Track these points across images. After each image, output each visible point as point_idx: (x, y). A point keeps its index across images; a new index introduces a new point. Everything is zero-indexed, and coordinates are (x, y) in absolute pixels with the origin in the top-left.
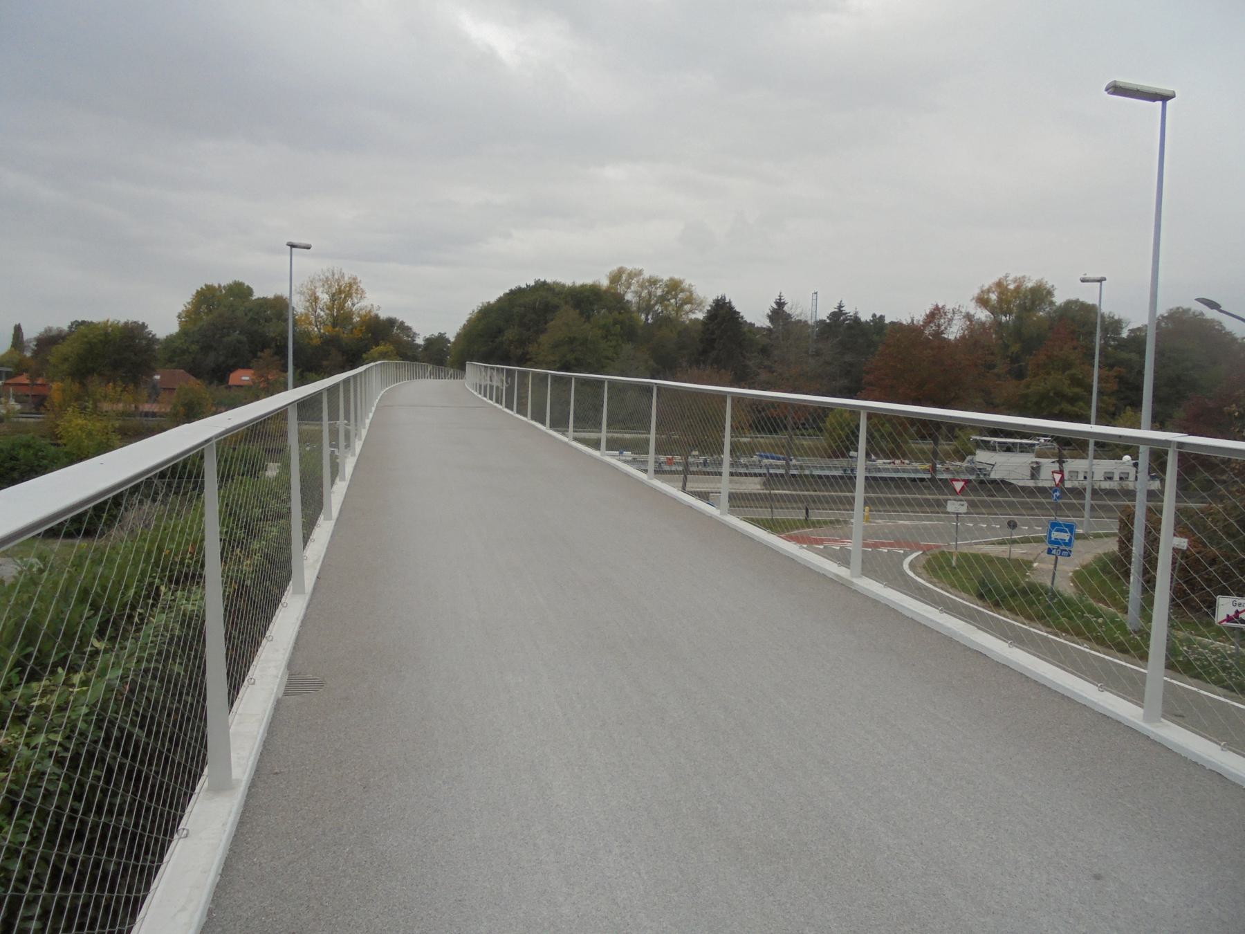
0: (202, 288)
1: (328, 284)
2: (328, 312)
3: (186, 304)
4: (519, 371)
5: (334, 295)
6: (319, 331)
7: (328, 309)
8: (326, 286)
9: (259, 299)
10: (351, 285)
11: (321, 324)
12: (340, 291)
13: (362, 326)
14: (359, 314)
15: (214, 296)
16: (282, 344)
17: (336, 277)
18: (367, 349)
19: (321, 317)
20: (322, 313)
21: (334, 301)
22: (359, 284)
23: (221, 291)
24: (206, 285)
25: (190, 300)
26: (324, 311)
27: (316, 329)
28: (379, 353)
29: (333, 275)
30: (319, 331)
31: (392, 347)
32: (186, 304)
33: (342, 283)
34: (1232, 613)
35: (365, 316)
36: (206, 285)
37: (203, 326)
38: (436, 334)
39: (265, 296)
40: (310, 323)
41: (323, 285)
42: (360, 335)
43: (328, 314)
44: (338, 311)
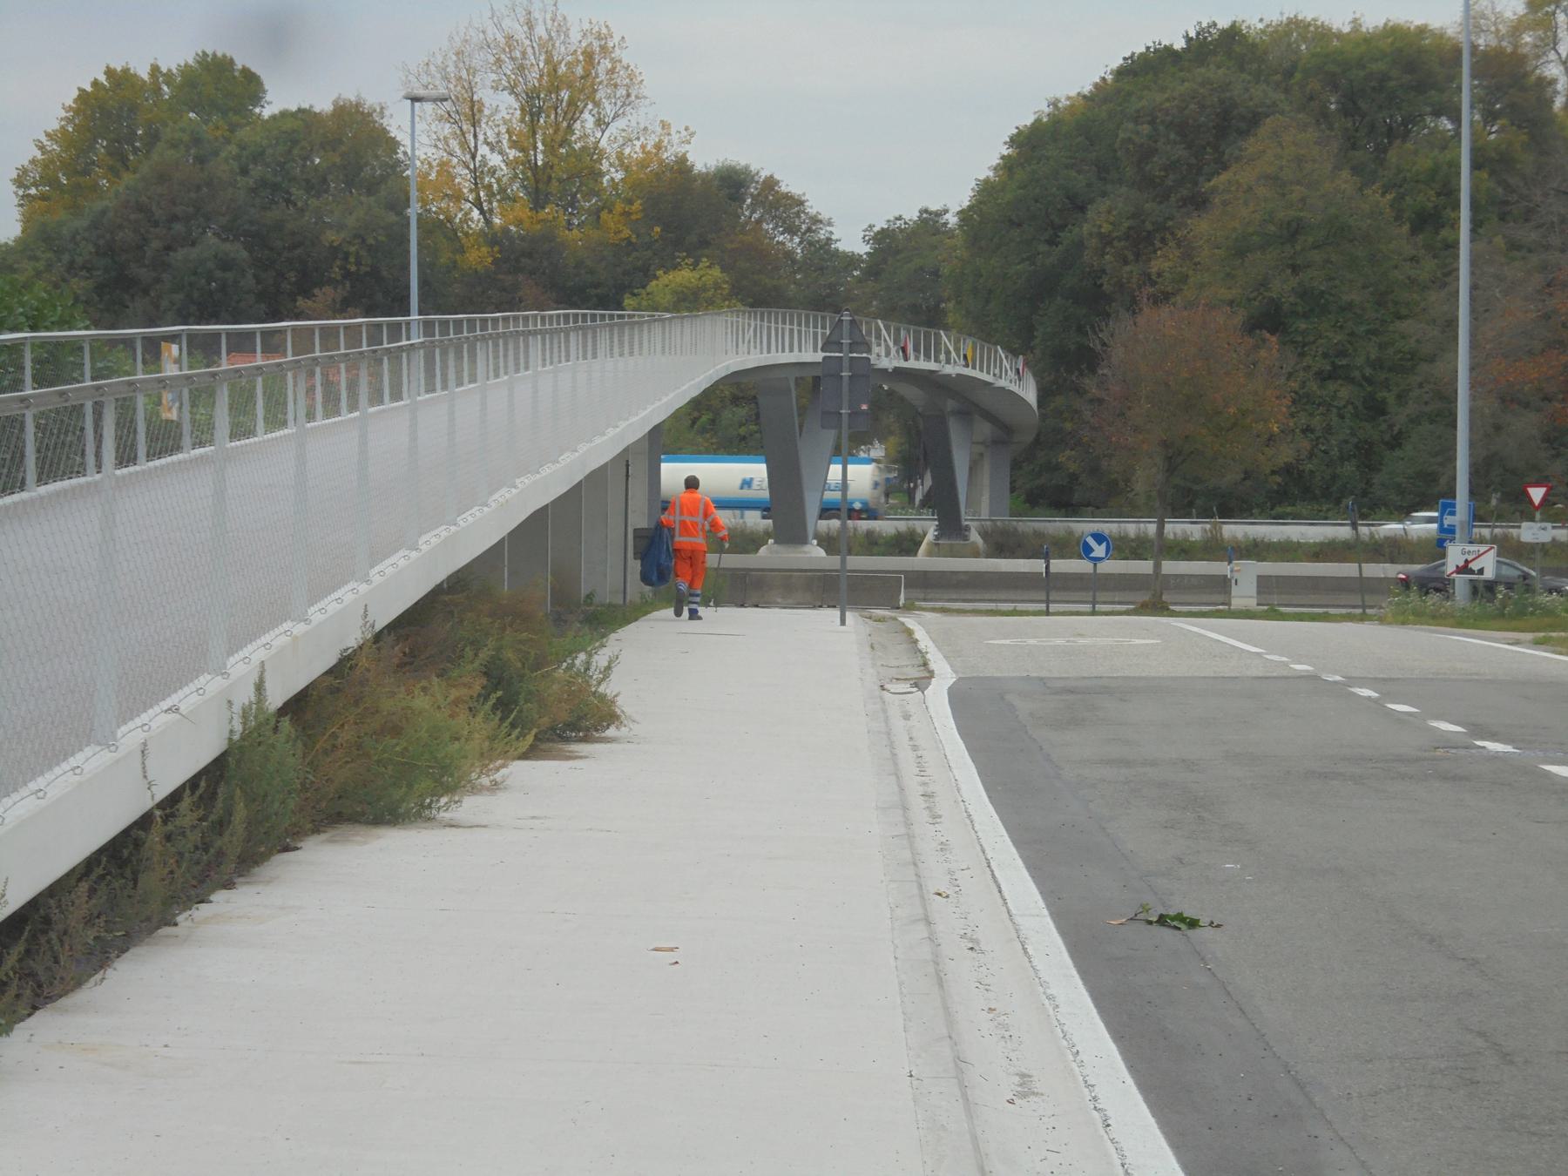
0: (95, 83)
1: (513, 59)
2: (513, 154)
3: (44, 139)
4: (229, 334)
5: (532, 95)
6: (488, 222)
7: (514, 144)
8: (508, 67)
9: (284, 114)
10: (589, 56)
11: (491, 195)
12: (554, 81)
13: (630, 202)
14: (620, 156)
15: (134, 109)
16: (364, 269)
17: (540, 31)
18: (645, 274)
19: (493, 171)
20: (495, 160)
21: (534, 116)
22: (617, 53)
23: (157, 91)
24: (109, 72)
25: (54, 125)
26: (501, 153)
27: (476, 214)
28: (675, 292)
29: (530, 25)
30: (488, 222)
31: (716, 272)
32: (44, 139)
33: (560, 51)
34: (1461, 564)
35: (643, 164)
36: (109, 72)
37: (104, 212)
38: (912, 215)
39: (305, 106)
40: (458, 197)
41: (499, 62)
42: (626, 233)
43: (516, 159)
44: (550, 149)
